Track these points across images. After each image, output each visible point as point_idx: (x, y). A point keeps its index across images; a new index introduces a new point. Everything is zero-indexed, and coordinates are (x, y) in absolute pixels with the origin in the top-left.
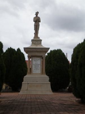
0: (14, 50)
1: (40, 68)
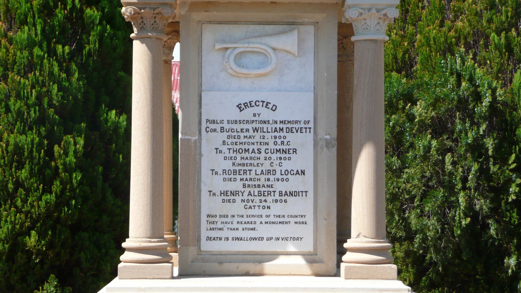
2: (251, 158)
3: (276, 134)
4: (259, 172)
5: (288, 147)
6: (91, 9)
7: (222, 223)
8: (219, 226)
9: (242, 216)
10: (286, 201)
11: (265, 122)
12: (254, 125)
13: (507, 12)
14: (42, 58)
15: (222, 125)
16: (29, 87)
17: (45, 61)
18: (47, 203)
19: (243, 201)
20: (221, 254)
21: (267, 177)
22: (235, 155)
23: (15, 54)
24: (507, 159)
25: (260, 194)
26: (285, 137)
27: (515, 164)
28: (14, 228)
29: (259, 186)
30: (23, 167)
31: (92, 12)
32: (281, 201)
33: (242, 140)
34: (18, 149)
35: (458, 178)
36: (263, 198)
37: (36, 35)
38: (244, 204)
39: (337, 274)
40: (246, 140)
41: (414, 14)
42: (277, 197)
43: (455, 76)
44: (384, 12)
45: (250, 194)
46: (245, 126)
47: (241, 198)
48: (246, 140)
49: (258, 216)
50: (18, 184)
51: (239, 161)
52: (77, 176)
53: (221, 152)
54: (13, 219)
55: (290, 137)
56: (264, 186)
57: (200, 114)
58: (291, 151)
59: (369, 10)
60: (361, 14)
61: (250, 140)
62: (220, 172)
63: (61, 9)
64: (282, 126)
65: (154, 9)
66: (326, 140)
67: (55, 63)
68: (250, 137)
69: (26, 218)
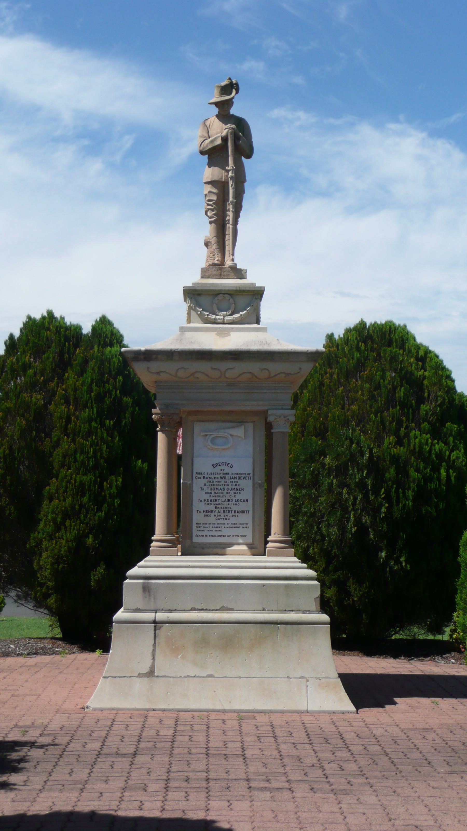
0: (78, 328)
1: (249, 506)
2: (219, 493)
3: (233, 480)
4: (223, 500)
5: (239, 487)
6: (127, 398)
7: (204, 527)
8: (203, 529)
9: (215, 524)
10: (238, 516)
11: (227, 474)
12: (221, 475)
13: (381, 401)
14: (96, 428)
15: (204, 475)
16: (89, 446)
17: (99, 430)
18: (99, 517)
19: (215, 516)
20: (203, 544)
21: (228, 503)
22: (211, 491)
23: (80, 426)
24: (380, 492)
25: (224, 512)
26: (237, 482)
27: (384, 495)
28: (79, 533)
29: (224, 508)
30: (85, 496)
31: (127, 399)
32: (235, 516)
33: (215, 483)
34: (82, 484)
35: (350, 503)
36: (226, 514)
37: (93, 414)
38: (215, 517)
39: (264, 554)
40: (217, 483)
41: (327, 400)
42: (233, 513)
43: (348, 441)
44: (288, 418)
45: (219, 512)
46: (216, 476)
47: (214, 514)
48: (217, 483)
49: (223, 524)
50: (81, 506)
51: (213, 494)
52: (117, 501)
53: (203, 489)
54: (78, 527)
55: (240, 482)
56: (226, 508)
57: (193, 469)
58: (241, 489)
59: (280, 417)
60: (276, 419)
61: (219, 483)
62: (203, 500)
63: (108, 398)
64: (236, 476)
65: (169, 416)
66: (259, 484)
67: (105, 432)
68: (219, 482)
69: (87, 526)
